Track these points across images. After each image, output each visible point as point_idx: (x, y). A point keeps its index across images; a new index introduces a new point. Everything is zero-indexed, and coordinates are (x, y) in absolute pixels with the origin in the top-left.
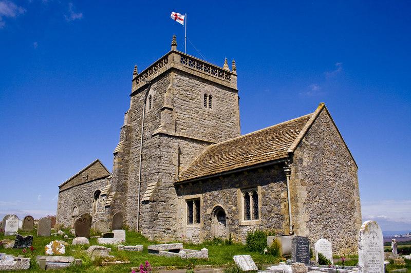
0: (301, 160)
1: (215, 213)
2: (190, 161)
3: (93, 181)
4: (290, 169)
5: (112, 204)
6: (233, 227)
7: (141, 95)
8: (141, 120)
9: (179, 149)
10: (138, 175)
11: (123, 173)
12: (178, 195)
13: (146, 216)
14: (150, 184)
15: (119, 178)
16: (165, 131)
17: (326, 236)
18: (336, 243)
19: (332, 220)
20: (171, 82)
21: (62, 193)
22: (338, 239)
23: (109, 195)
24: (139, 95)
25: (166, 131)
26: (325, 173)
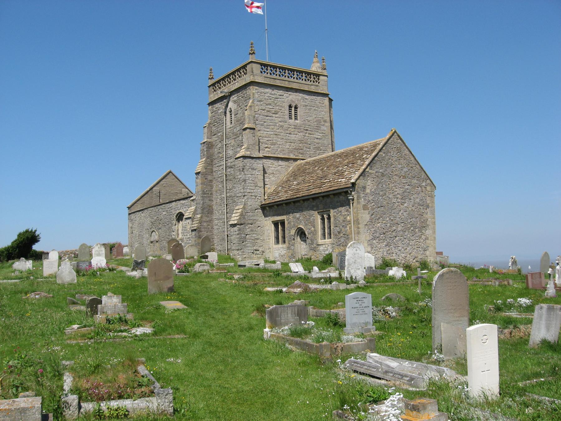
0: (364, 188)
1: (298, 233)
2: (276, 180)
3: (173, 201)
4: (353, 196)
5: (198, 228)
6: (313, 246)
7: (220, 106)
8: (223, 136)
9: (264, 170)
10: (223, 196)
11: (207, 194)
12: (265, 216)
13: (234, 238)
14: (237, 208)
15: (203, 200)
16: (248, 153)
17: (389, 252)
18: (401, 258)
19: (397, 238)
20: (251, 97)
21: (133, 215)
22: (403, 255)
23: (194, 218)
24: (218, 105)
25: (249, 153)
26: (390, 196)
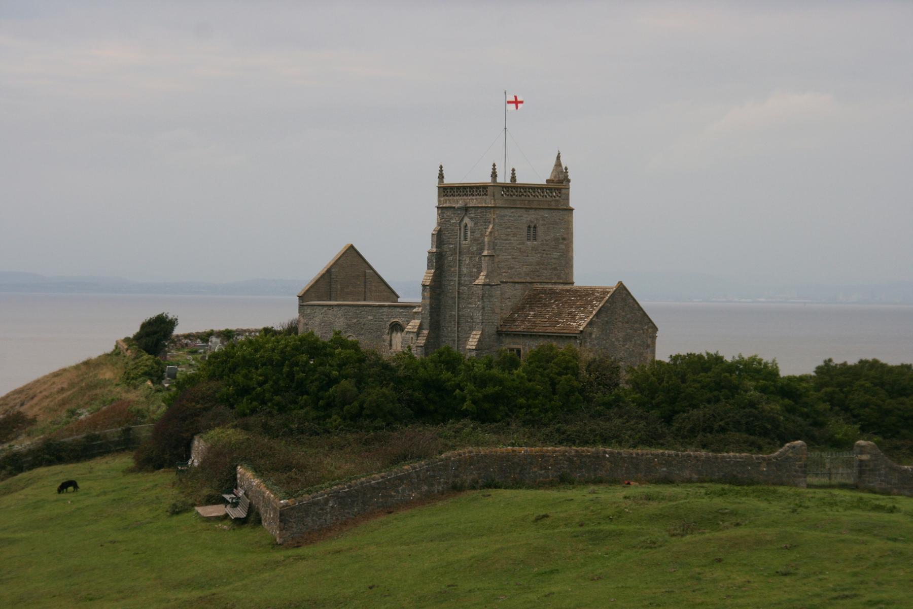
0: (591, 334)
